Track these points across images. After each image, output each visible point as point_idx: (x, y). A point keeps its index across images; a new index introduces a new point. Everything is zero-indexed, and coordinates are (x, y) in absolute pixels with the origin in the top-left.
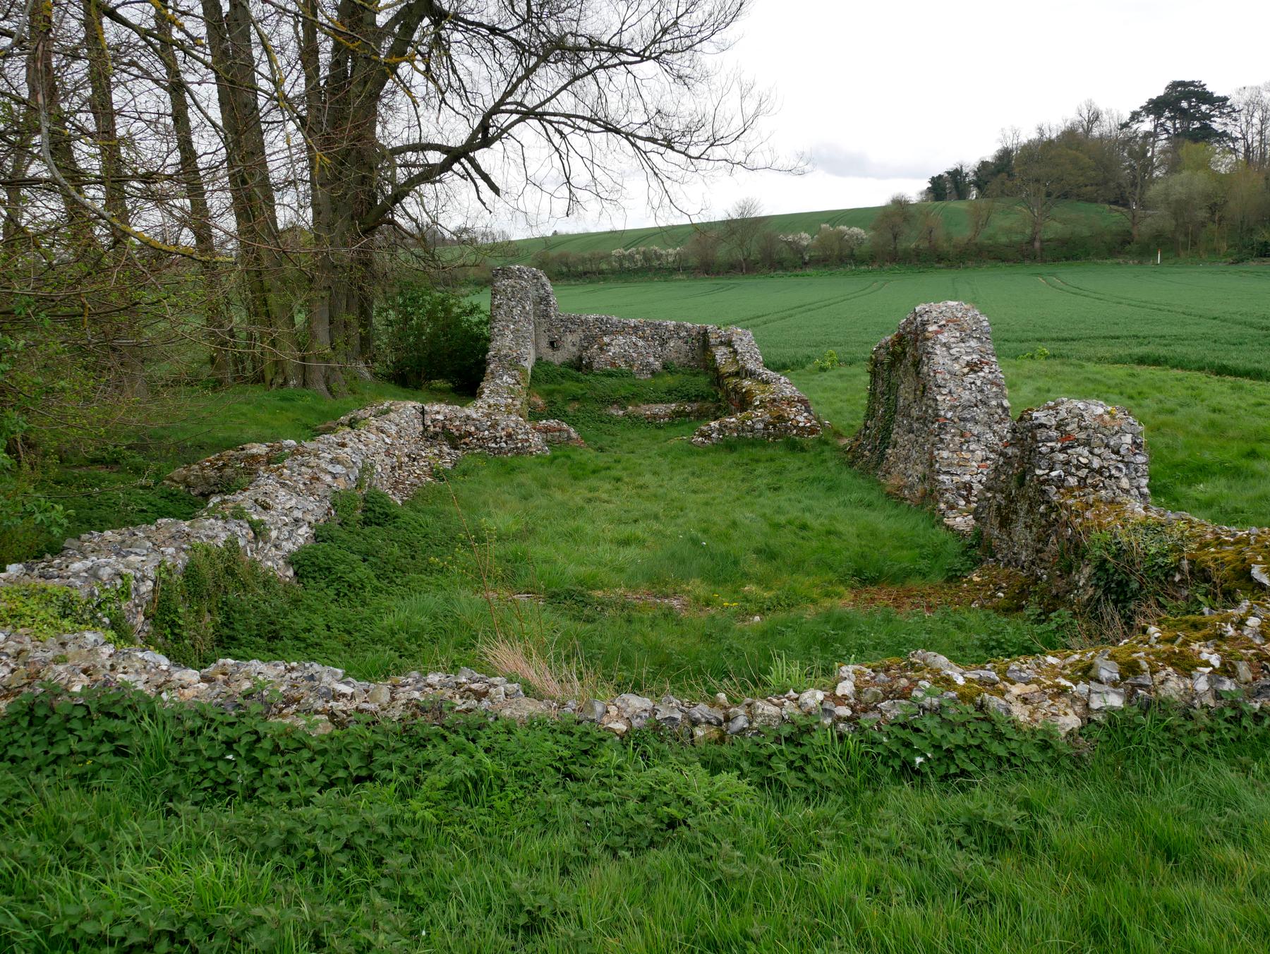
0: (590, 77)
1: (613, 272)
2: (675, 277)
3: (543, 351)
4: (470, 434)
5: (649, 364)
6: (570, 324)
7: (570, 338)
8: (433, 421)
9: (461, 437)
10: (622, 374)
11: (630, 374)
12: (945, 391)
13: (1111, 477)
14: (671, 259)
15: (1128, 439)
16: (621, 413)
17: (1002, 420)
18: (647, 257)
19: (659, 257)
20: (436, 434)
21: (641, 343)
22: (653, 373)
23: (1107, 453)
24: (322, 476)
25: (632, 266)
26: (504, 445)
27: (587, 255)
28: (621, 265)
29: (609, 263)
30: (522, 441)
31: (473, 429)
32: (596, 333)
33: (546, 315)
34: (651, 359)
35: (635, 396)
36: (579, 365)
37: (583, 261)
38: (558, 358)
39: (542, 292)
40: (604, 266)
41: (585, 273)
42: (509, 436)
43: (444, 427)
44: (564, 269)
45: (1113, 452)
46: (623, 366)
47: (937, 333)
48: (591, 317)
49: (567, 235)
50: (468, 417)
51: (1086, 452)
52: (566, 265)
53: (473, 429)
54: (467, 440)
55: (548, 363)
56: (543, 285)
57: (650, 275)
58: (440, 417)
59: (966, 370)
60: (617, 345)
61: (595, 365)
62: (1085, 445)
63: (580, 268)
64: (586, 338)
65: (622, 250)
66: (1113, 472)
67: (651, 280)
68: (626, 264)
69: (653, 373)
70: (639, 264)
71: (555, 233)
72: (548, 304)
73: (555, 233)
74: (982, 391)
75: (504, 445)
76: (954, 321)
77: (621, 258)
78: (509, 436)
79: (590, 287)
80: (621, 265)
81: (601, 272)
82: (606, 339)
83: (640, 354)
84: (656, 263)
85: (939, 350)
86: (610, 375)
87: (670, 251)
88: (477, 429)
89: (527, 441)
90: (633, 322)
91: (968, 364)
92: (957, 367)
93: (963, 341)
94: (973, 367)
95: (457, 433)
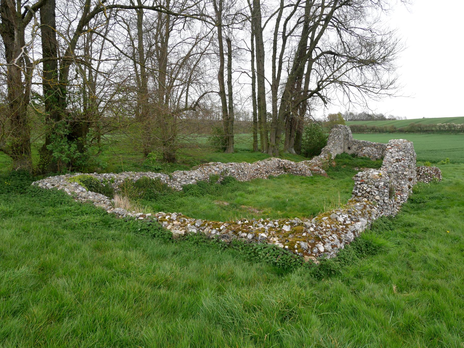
0: (99, 70)
1: (437, 131)
2: (459, 133)
3: (346, 150)
4: (290, 168)
5: (375, 156)
6: (354, 142)
7: (354, 147)
8: (282, 164)
9: (287, 169)
10: (366, 158)
11: (369, 159)
12: (384, 167)
13: (372, 194)
14: (459, 128)
15: (382, 184)
16: (358, 169)
17: (403, 178)
18: (450, 126)
19: (454, 127)
20: (281, 167)
21: (375, 150)
22: (377, 159)
23: (373, 187)
24: (212, 170)
25: (444, 129)
26: (298, 172)
27: (428, 125)
28: (440, 129)
29: (436, 128)
30: (304, 172)
31: (291, 167)
32: (361, 146)
33: (348, 139)
34: (377, 155)
35: (364, 165)
36: (354, 155)
37: (426, 127)
38: (350, 152)
39: (347, 133)
40: (434, 129)
41: (426, 131)
42: (300, 170)
43: (284, 166)
44: (419, 129)
45: (376, 187)
46: (367, 156)
47: (390, 148)
48: (361, 141)
49: (428, 118)
50: (290, 164)
51: (366, 186)
52: (420, 128)
53: (291, 167)
54: (289, 170)
55: (347, 154)
56: (348, 131)
57: (450, 132)
58: (283, 163)
59: (395, 161)
60: (367, 150)
61: (359, 155)
62: (366, 183)
63: (425, 129)
64: (359, 147)
65: (440, 124)
66: (373, 193)
67: (450, 134)
68: (442, 129)
69: (377, 159)
70: (447, 129)
71: (424, 118)
72: (348, 136)
73: (424, 118)
74: (397, 168)
75: (298, 172)
76: (397, 146)
77: (440, 127)
78: (300, 170)
79: (427, 135)
80: (440, 129)
81: (432, 131)
82: (364, 148)
83: (373, 153)
84: (453, 129)
85: (388, 154)
86: (362, 158)
87: (459, 125)
88: (292, 167)
89: (305, 172)
90: (374, 143)
91: (397, 159)
92: (392, 160)
93: (397, 152)
94: (398, 160)
95: (286, 168)
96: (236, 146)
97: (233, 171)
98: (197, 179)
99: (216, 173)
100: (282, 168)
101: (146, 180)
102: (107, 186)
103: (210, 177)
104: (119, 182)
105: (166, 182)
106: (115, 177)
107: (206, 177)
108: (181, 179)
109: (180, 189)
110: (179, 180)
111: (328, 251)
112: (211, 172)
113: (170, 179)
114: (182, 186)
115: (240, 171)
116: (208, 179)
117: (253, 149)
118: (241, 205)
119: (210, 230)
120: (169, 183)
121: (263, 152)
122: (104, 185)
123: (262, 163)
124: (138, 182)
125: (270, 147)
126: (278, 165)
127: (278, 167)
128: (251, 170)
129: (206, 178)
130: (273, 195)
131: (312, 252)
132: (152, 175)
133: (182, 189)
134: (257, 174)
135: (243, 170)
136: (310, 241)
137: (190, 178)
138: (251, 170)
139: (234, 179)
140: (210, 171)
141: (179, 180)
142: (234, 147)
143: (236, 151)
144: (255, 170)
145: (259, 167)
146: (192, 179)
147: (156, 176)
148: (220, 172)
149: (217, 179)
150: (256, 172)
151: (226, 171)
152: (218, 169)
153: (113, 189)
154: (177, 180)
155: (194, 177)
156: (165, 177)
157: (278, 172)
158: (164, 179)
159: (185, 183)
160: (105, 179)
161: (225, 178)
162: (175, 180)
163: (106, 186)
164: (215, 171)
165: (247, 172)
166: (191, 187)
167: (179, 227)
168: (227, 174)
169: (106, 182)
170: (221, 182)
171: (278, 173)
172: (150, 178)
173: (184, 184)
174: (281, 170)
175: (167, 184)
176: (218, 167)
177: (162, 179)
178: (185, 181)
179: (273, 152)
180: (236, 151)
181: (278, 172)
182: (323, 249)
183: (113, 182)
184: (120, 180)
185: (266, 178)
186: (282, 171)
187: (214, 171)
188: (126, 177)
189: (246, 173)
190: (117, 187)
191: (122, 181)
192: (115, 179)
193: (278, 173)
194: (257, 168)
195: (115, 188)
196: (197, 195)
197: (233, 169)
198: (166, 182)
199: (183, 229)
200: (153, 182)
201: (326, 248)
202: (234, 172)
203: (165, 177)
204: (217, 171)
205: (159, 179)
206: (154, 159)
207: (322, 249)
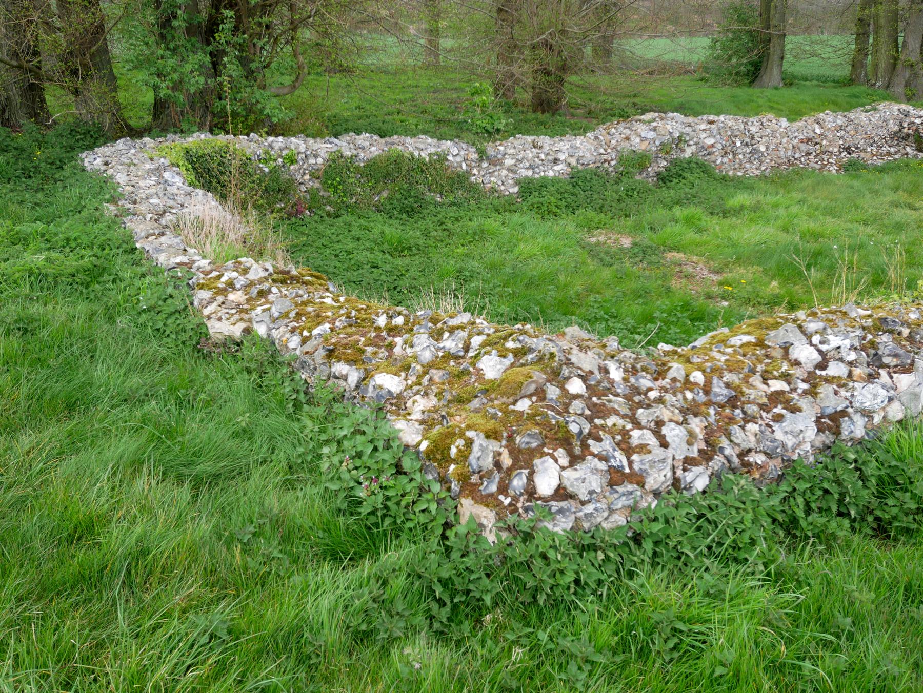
20: (908, 135)
43: (917, 130)
96: (791, 65)
97: (710, 141)
98: (573, 162)
99: (643, 147)
100: (911, 139)
101: (398, 161)
102: (274, 171)
103: (621, 160)
104: (312, 161)
105: (464, 166)
106: (302, 148)
107: (605, 157)
108: (518, 160)
109: (511, 190)
110: (509, 162)
111: (571, 496)
112: (627, 144)
113: (481, 159)
114: (517, 182)
115: (738, 144)
116: (613, 163)
117: (851, 75)
118: (671, 249)
119: (288, 335)
120: (475, 171)
121: (875, 84)
122: (267, 170)
123: (831, 119)
124: (372, 164)
125: (899, 66)
126: (896, 128)
127: (896, 133)
128: (784, 141)
129: (605, 161)
130: (805, 224)
131: (503, 489)
132: (422, 146)
133: (516, 189)
134: (808, 154)
135: (753, 138)
136: (518, 439)
137: (551, 158)
138: (784, 141)
139: (704, 169)
140: (627, 139)
141: (509, 162)
142: (785, 67)
143: (789, 81)
144: (802, 141)
145: (818, 131)
146: (556, 161)
147: (433, 150)
148: (658, 143)
149: (642, 168)
150: (803, 147)
151: (680, 141)
152: (651, 135)
153: (292, 181)
154: (502, 164)
155: (562, 157)
156: (462, 153)
157: (892, 150)
158: (458, 159)
159: (530, 173)
160: (267, 153)
161: (674, 163)
162: (496, 162)
163: (270, 172)
164: (643, 139)
165: (767, 148)
166: (543, 185)
167: (234, 311)
168: (683, 151)
169: (271, 159)
170: (658, 174)
171: (889, 154)
172: (412, 154)
173: (527, 177)
174: (904, 143)
175: (469, 173)
176: (655, 129)
177: (450, 158)
178: (531, 167)
179: (907, 84)
180: (789, 81)
181: (892, 150)
182: (555, 483)
183: (293, 161)
184: (316, 156)
185: (833, 169)
186: (908, 149)
187: (638, 140)
188: (335, 149)
189: (763, 149)
190: (307, 177)
191: (320, 160)
192: (299, 153)
193: (889, 154)
194: (811, 135)
195: (299, 177)
196: (555, 210)
197: (711, 136)
198: (464, 166)
199: (242, 319)
200: (421, 167)
201: (566, 483)
202: (713, 146)
203: (462, 153)
204: (646, 139)
205: (442, 158)
206: (483, 103)
207: (546, 484)
